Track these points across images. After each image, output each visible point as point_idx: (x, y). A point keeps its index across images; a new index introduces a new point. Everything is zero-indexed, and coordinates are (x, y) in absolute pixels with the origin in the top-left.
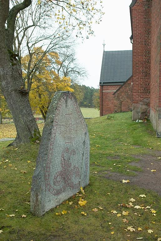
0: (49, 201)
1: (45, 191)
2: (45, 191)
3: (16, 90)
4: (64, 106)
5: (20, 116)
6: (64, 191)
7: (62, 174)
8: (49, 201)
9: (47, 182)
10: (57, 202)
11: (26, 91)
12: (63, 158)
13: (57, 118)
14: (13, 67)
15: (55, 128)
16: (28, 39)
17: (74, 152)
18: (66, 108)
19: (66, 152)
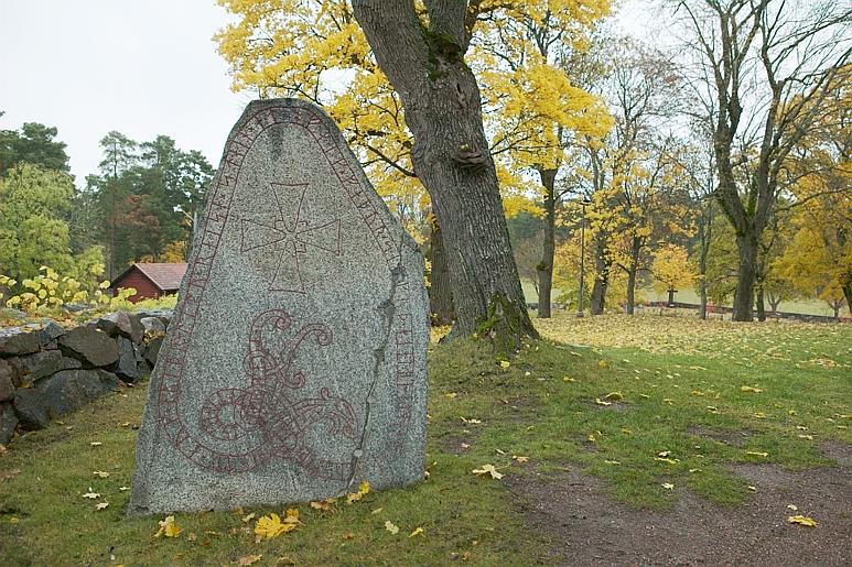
0: (171, 482)
1: (156, 442)
2: (156, 442)
3: (442, 158)
4: (265, 150)
5: (457, 244)
6: (255, 470)
7: (247, 403)
8: (171, 482)
9: (168, 411)
10: (215, 498)
11: (471, 160)
12: (258, 343)
13: (224, 191)
14: (432, 83)
15: (215, 226)
16: (767, 33)
17: (322, 334)
18: (274, 159)
19: (275, 326)
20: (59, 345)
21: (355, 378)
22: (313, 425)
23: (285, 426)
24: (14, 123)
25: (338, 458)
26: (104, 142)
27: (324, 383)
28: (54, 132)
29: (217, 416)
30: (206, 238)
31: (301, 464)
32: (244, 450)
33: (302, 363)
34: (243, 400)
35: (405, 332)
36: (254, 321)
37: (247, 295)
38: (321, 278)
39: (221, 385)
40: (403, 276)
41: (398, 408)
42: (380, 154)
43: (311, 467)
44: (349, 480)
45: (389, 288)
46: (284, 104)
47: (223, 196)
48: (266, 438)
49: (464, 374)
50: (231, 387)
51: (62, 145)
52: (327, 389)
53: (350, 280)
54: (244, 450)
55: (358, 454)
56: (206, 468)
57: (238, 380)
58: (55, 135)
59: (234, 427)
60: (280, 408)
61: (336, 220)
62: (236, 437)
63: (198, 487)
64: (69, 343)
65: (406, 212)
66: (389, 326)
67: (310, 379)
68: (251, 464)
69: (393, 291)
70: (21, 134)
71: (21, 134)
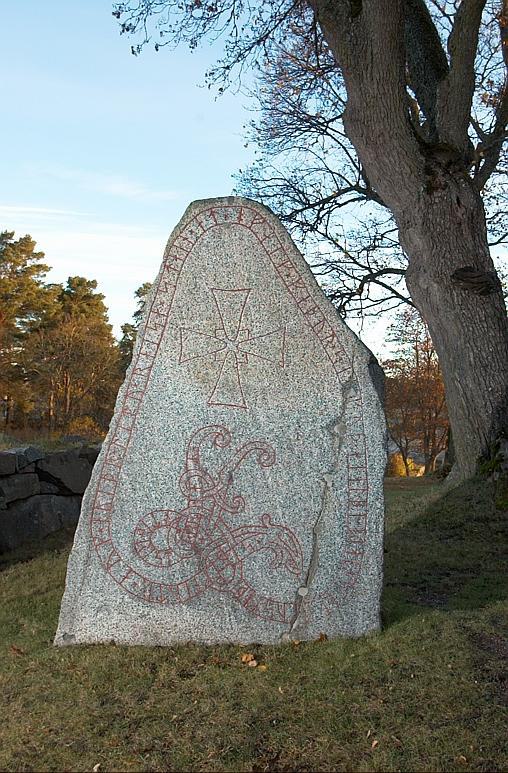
2: (87, 563)
6: (189, 602)
7: (182, 525)
9: (101, 531)
12: (196, 461)
14: (428, 197)
19: (214, 443)
20: (36, 468)
21: (300, 505)
23: (222, 556)
24: (57, 276)
25: (280, 596)
26: (139, 293)
28: (93, 284)
30: (144, 347)
32: (178, 578)
33: (242, 483)
34: (180, 524)
35: (357, 455)
36: (192, 437)
37: (185, 409)
40: (356, 391)
41: (349, 543)
42: (393, 291)
43: (247, 602)
44: (292, 623)
45: (340, 404)
46: (226, 203)
47: (162, 303)
48: (202, 567)
49: (458, 518)
50: (166, 508)
51: (101, 296)
54: (178, 578)
55: (303, 592)
57: (173, 502)
58: (95, 287)
59: (168, 552)
62: (170, 564)
63: (128, 617)
64: (47, 468)
65: (433, 358)
66: (340, 447)
67: (251, 504)
68: (184, 595)
69: (344, 407)
70: (65, 286)
71: (65, 286)
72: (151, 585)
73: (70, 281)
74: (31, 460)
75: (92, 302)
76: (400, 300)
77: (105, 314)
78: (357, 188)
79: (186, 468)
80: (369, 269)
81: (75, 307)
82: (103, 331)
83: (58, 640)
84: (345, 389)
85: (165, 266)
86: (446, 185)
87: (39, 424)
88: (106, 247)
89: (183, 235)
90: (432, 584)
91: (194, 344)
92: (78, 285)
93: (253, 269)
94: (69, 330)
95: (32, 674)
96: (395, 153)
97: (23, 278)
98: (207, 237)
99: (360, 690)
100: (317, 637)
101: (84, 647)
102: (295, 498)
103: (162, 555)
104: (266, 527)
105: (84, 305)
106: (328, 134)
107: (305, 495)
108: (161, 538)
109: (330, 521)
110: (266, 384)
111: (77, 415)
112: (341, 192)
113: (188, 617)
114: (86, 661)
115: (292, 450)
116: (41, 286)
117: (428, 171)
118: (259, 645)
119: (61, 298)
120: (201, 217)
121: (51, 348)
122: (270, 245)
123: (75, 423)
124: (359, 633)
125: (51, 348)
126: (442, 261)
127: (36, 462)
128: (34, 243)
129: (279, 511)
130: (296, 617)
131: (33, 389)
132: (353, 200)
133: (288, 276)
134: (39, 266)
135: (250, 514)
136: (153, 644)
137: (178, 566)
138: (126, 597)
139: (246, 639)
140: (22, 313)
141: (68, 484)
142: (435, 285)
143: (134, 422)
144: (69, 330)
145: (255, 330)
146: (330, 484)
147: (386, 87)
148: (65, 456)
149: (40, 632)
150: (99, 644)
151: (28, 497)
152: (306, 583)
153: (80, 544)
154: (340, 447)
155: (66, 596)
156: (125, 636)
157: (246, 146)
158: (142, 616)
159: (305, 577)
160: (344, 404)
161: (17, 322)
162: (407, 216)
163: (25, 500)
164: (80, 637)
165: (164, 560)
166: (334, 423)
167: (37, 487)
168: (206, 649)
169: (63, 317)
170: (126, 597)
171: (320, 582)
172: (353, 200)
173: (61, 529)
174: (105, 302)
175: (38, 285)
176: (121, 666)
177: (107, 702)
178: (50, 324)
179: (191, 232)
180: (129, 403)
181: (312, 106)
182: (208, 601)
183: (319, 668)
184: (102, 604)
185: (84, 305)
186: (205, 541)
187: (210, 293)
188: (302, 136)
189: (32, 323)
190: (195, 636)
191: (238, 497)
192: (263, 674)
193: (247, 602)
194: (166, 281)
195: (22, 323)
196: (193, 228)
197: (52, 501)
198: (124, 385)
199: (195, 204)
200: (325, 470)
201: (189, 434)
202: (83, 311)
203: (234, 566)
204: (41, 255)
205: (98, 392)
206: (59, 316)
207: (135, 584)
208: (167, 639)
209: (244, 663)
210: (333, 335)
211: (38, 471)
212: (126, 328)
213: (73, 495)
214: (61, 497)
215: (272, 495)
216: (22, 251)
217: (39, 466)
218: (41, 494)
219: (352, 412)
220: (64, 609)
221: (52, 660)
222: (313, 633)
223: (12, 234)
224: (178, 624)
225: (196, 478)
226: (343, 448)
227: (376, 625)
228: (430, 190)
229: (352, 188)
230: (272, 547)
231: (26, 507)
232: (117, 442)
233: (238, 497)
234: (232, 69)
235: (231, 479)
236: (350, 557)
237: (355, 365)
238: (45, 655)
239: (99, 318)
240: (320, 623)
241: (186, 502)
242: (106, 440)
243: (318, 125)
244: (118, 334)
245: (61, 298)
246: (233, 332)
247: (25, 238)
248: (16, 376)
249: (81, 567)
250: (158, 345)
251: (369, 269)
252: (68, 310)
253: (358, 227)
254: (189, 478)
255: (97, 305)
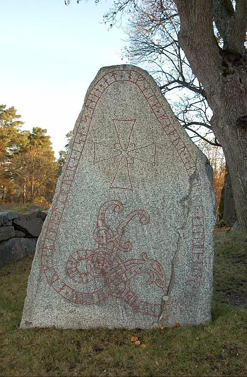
2: (39, 280)
9: (47, 261)
12: (103, 221)
19: (114, 211)
20: (13, 223)
21: (165, 247)
22: (136, 276)
24: (27, 127)
25: (152, 301)
26: (67, 136)
27: (144, 249)
28: (45, 131)
29: (76, 267)
31: (127, 302)
33: (130, 234)
34: (94, 258)
35: (198, 218)
36: (101, 207)
38: (143, 180)
39: (79, 247)
40: (198, 180)
41: (193, 270)
43: (133, 304)
44: (159, 316)
45: (188, 188)
46: (122, 68)
48: (106, 284)
51: (49, 137)
52: (145, 253)
53: (162, 182)
55: (166, 298)
56: (69, 301)
57: (90, 244)
58: (46, 132)
59: (86, 274)
60: (115, 264)
61: (153, 143)
64: (19, 223)
66: (188, 213)
67: (135, 246)
68: (96, 300)
69: (190, 190)
70: (31, 132)
71: (31, 132)
72: (76, 293)
73: (34, 129)
74: (10, 219)
75: (44, 140)
76: (200, 138)
77: (51, 146)
78: (178, 81)
79: (97, 225)
80: (185, 122)
81: (36, 142)
82: (50, 154)
83: (23, 325)
84: (191, 179)
85: (86, 106)
86: (234, 72)
87: (19, 199)
88: (52, 112)
89: (96, 87)
90: (234, 290)
91: (103, 152)
92: (38, 131)
93: (137, 108)
94: (33, 154)
95: (7, 348)
96: (206, 54)
97: (10, 128)
98: (110, 88)
99: (206, 365)
100: (173, 324)
101: (37, 330)
102: (161, 243)
103: (83, 276)
104: (144, 260)
105: (41, 141)
106: (164, 53)
107: (167, 241)
108: (82, 266)
109: (183, 259)
110: (144, 176)
111: (37, 195)
112: (170, 83)
113: (98, 312)
114: (39, 339)
115: (160, 215)
116: (19, 132)
117: (224, 64)
118: (140, 329)
119: (29, 138)
120: (107, 77)
121: (24, 162)
122: (147, 94)
123: (36, 199)
124: (198, 322)
125: (24, 162)
126: (231, 113)
127: (13, 220)
128: (16, 111)
129: (152, 251)
130: (161, 312)
131: (15, 183)
132: (176, 87)
133: (158, 112)
134: (18, 122)
135: (135, 252)
136: (77, 328)
137: (92, 282)
138: (62, 300)
139: (132, 326)
140: (10, 146)
141: (31, 231)
142: (227, 126)
143: (67, 198)
144: (33, 154)
145: (138, 144)
146: (182, 235)
147: (202, 19)
148: (29, 217)
149: (12, 319)
150: (46, 328)
151: (9, 239)
152: (168, 293)
153: (35, 268)
154: (188, 213)
155: (27, 300)
156: (61, 323)
157: (122, 59)
158: (71, 312)
159: (167, 289)
160: (191, 187)
161: (8, 150)
162: (212, 89)
163: (7, 240)
164: (36, 324)
165: (84, 279)
166: (185, 199)
167: (13, 233)
168: (109, 332)
169: (30, 147)
170: (62, 300)
171: (176, 292)
172: (176, 87)
173: (27, 256)
174: (51, 140)
175: (18, 131)
176: (59, 343)
177: (50, 370)
178: (24, 150)
179: (101, 85)
180: (65, 187)
181: (157, 38)
182: (109, 303)
183: (178, 346)
184: (49, 306)
185: (41, 141)
186: (108, 269)
187: (112, 122)
188: (150, 55)
189: (15, 150)
190: (102, 323)
191: (128, 242)
192: (145, 350)
193: (133, 304)
194: (86, 115)
195: (11, 150)
196: (102, 83)
197: (22, 240)
198: (61, 176)
199: (103, 69)
200: (179, 227)
201: (99, 205)
202: (40, 144)
203: (125, 283)
204: (19, 116)
205: (48, 185)
206: (28, 147)
207: (67, 293)
208: (86, 325)
209: (132, 342)
210: (185, 147)
211: (14, 224)
212: (61, 153)
213: (32, 237)
214: (27, 239)
215: (147, 241)
216: (10, 114)
217: (15, 222)
218: (16, 237)
219: (195, 192)
220: (26, 307)
221: (18, 339)
222: (171, 322)
223: (5, 106)
224: (93, 316)
225: (103, 231)
226: (190, 214)
227: (209, 318)
228: (225, 74)
229: (175, 81)
230: (147, 271)
231: (7, 244)
232: (57, 210)
233: (128, 242)
234: (117, 14)
235: (123, 232)
236: (193, 278)
237: (198, 165)
238: (14, 336)
239: (48, 148)
240: (176, 317)
241: (97, 245)
242: (51, 208)
243: (161, 49)
244: (57, 156)
245: (29, 138)
246: (125, 145)
247: (12, 108)
248: (7, 176)
249: (36, 282)
250: (81, 153)
251: (185, 122)
252: (33, 143)
253: (178, 100)
254: (99, 231)
255: (47, 141)
